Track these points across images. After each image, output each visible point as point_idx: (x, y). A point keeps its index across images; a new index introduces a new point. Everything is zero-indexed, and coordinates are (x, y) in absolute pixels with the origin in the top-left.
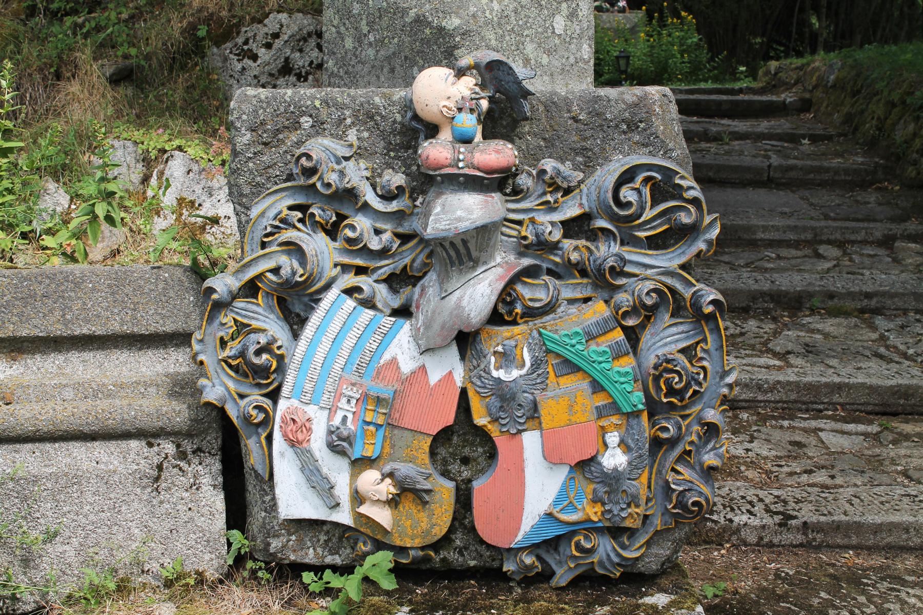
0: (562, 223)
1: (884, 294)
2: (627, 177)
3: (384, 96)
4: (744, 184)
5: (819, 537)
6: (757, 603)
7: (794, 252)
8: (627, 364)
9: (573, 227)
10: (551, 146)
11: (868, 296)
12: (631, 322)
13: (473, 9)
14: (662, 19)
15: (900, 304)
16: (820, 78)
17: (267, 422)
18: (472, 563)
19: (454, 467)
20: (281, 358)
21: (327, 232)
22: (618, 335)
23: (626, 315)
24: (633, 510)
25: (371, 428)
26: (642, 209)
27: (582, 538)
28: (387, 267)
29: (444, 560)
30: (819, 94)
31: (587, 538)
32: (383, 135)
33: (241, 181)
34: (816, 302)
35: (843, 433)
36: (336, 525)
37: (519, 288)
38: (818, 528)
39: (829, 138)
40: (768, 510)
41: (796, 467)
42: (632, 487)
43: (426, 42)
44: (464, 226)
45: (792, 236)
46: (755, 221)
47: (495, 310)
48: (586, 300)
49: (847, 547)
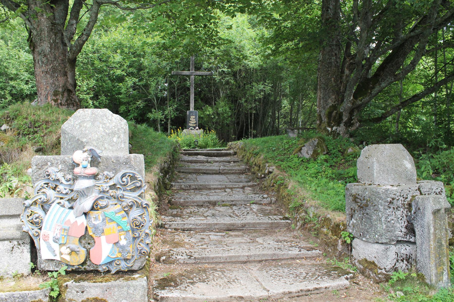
0: (110, 186)
1: (236, 201)
2: (123, 176)
3: (68, 157)
4: (213, 174)
5: (199, 261)
6: (176, 277)
7: (219, 191)
8: (126, 219)
9: (113, 187)
10: (107, 168)
11: (232, 201)
12: (126, 209)
13: (90, 137)
14: (206, 132)
15: (240, 203)
16: (239, 147)
17: (38, 236)
18: (92, 269)
19: (87, 245)
20: (42, 220)
21: (53, 189)
22: (123, 213)
23: (124, 208)
24: (129, 254)
25: (64, 236)
26: (128, 182)
28: (68, 197)
29: (85, 268)
30: (238, 151)
31: (118, 261)
32: (67, 166)
33: (33, 177)
34: (219, 203)
35: (216, 235)
37: (99, 202)
38: (198, 259)
39: (238, 162)
40: (187, 255)
41: (200, 244)
42: (128, 249)
43: (79, 144)
44: (82, 187)
45: (220, 187)
46: (212, 183)
47: (93, 207)
48: (116, 204)
49: (206, 263)
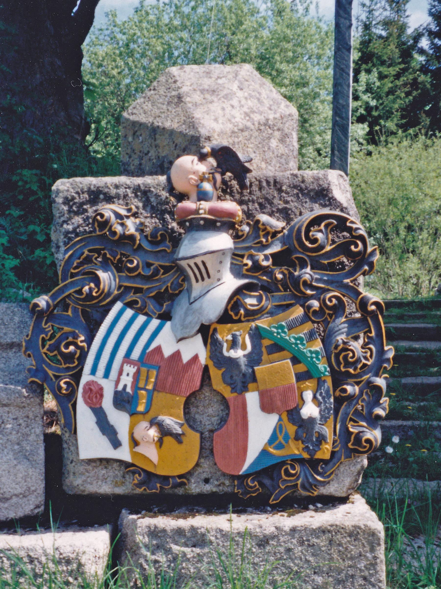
27: (289, 467)
36: (120, 462)
